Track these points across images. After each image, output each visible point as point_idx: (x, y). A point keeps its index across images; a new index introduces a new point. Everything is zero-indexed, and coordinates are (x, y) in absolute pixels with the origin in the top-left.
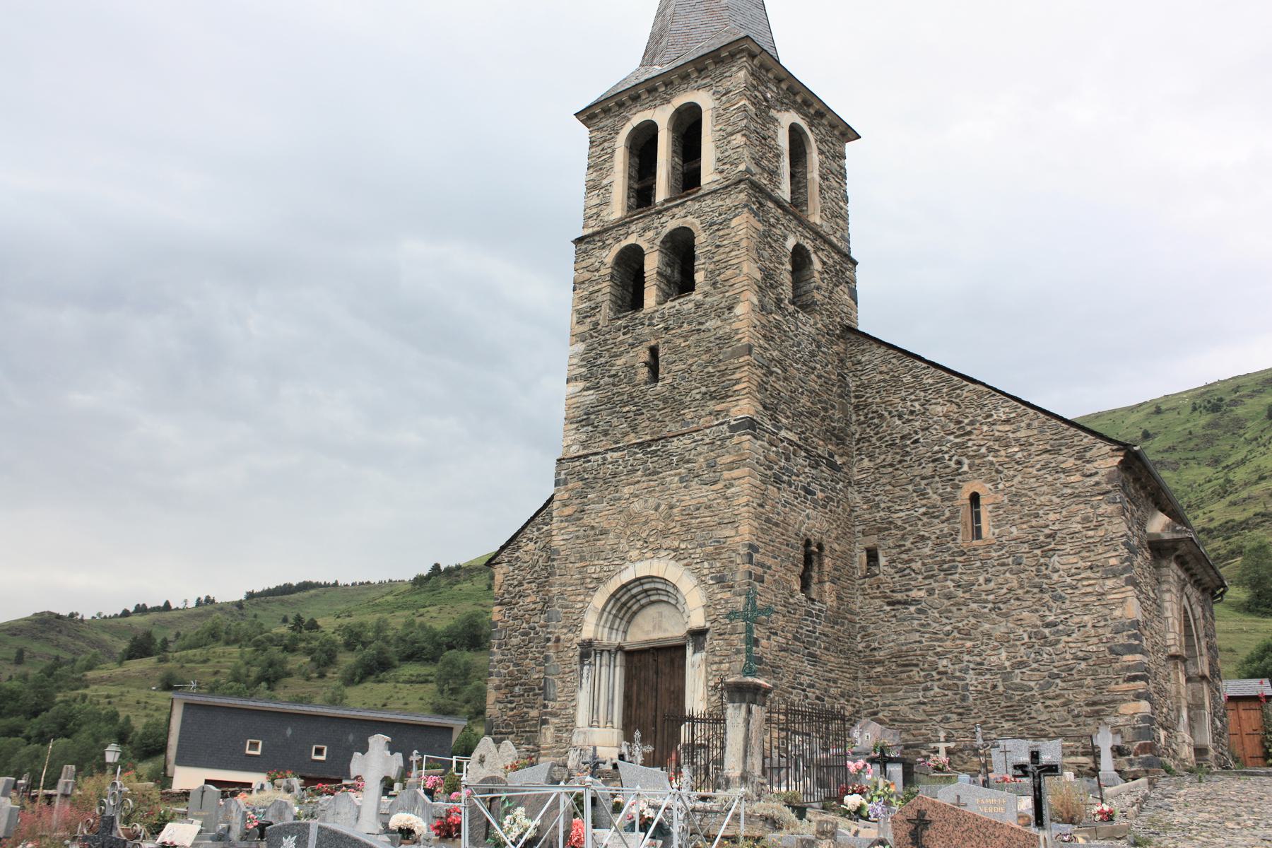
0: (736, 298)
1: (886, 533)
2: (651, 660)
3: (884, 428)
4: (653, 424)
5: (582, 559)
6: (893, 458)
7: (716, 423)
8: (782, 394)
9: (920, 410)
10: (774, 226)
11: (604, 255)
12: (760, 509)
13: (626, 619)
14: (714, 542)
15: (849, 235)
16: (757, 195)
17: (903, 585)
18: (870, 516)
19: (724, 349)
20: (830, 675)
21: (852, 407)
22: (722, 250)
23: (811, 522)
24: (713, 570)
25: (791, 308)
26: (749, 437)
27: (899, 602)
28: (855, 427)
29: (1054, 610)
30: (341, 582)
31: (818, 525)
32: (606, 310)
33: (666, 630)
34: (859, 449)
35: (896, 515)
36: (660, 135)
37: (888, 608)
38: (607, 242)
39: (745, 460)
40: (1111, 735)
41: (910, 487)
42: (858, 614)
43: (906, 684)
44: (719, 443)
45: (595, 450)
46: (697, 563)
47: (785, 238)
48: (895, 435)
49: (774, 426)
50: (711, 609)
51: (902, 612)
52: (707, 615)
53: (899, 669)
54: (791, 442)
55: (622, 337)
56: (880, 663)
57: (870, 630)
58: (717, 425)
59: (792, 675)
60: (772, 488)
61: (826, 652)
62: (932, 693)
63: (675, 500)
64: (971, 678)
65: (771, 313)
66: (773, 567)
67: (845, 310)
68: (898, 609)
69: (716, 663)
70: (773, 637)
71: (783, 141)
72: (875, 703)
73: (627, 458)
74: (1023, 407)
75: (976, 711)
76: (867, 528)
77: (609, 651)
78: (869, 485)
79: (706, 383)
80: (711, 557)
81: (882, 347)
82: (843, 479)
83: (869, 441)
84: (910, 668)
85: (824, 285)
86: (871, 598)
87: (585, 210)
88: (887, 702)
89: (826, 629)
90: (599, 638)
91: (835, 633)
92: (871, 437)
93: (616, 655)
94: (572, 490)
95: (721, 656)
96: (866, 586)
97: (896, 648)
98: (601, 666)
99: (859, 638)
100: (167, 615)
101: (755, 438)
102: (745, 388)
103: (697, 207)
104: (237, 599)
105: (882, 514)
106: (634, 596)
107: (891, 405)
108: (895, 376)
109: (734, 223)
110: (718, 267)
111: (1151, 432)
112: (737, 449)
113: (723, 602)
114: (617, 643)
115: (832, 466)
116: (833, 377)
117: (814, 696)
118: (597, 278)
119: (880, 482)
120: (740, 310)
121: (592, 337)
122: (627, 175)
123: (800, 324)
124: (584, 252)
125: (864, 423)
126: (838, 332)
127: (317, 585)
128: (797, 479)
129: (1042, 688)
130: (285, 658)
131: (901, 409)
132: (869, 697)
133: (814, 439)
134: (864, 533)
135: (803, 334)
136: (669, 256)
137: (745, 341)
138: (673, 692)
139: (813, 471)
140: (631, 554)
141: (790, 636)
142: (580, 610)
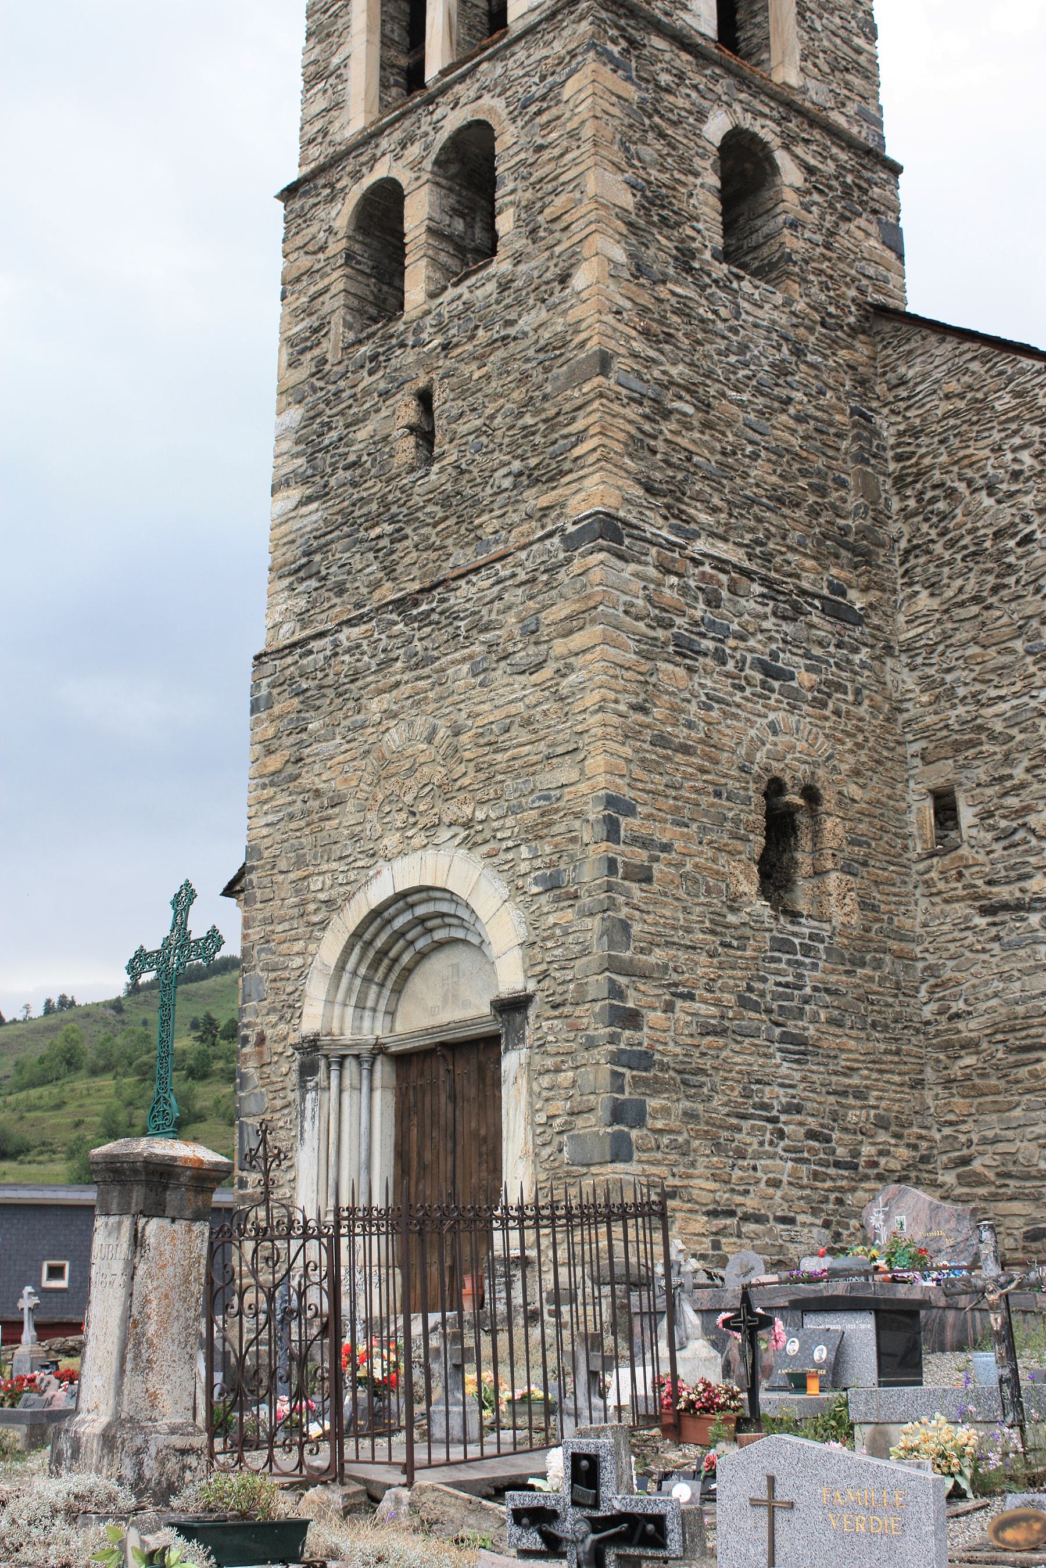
0: (575, 253)
1: (971, 753)
2: (442, 1072)
3: (959, 518)
4: (425, 555)
5: (300, 862)
7: (540, 533)
8: (695, 459)
9: (1032, 467)
10: (668, 90)
11: (333, 214)
12: (640, 717)
13: (390, 984)
14: (540, 798)
15: (880, 109)
16: (622, 22)
17: (1013, 868)
18: (935, 718)
19: (555, 371)
20: (847, 1081)
21: (890, 482)
22: (546, 155)
23: (782, 738)
24: (538, 863)
25: (721, 270)
26: (602, 556)
27: (1005, 907)
28: (899, 524)
31: (801, 745)
32: (338, 331)
33: (466, 1004)
34: (906, 572)
35: (988, 712)
37: (981, 921)
38: (339, 186)
39: (595, 608)
41: (1019, 645)
42: (917, 940)
43: (1029, 1091)
44: (545, 577)
45: (321, 628)
46: (508, 849)
47: (702, 116)
48: (982, 532)
49: (676, 530)
50: (537, 950)
51: (1012, 927)
53: (1012, 1059)
54: (721, 564)
55: (368, 380)
56: (970, 1045)
57: (947, 974)
58: (541, 539)
59: (739, 1088)
60: (670, 667)
61: (833, 1029)
63: (464, 715)
65: (664, 282)
66: (678, 845)
67: (871, 271)
68: (1003, 923)
69: (548, 1071)
70: (679, 1004)
72: (963, 1138)
73: (376, 636)
76: (931, 746)
77: (357, 1057)
78: (931, 648)
79: (519, 451)
80: (534, 834)
81: (949, 339)
82: (870, 641)
83: (928, 552)
86: (946, 901)
87: (302, 129)
88: (990, 1134)
89: (833, 978)
90: (336, 1030)
92: (932, 541)
93: (372, 1065)
94: (280, 717)
96: (934, 874)
97: (1003, 1010)
98: (341, 1091)
99: (923, 994)
101: (621, 557)
102: (594, 450)
103: (499, 71)
104: (113, 997)
105: (961, 710)
106: (400, 934)
107: (971, 465)
108: (977, 401)
109: (567, 92)
110: (539, 195)
112: (578, 585)
114: (370, 1038)
116: (838, 417)
117: (802, 1131)
118: (322, 264)
119: (953, 640)
120: (580, 280)
121: (314, 390)
122: (377, 38)
123: (745, 305)
124: (299, 216)
126: (852, 319)
128: (742, 645)
130: (191, 1089)
131: (991, 472)
132: (951, 1123)
133: (790, 556)
134: (924, 757)
135: (756, 326)
136: (459, 195)
137: (592, 346)
138: (485, 1140)
139: (787, 627)
140: (385, 841)
141: (729, 998)
142: (298, 973)
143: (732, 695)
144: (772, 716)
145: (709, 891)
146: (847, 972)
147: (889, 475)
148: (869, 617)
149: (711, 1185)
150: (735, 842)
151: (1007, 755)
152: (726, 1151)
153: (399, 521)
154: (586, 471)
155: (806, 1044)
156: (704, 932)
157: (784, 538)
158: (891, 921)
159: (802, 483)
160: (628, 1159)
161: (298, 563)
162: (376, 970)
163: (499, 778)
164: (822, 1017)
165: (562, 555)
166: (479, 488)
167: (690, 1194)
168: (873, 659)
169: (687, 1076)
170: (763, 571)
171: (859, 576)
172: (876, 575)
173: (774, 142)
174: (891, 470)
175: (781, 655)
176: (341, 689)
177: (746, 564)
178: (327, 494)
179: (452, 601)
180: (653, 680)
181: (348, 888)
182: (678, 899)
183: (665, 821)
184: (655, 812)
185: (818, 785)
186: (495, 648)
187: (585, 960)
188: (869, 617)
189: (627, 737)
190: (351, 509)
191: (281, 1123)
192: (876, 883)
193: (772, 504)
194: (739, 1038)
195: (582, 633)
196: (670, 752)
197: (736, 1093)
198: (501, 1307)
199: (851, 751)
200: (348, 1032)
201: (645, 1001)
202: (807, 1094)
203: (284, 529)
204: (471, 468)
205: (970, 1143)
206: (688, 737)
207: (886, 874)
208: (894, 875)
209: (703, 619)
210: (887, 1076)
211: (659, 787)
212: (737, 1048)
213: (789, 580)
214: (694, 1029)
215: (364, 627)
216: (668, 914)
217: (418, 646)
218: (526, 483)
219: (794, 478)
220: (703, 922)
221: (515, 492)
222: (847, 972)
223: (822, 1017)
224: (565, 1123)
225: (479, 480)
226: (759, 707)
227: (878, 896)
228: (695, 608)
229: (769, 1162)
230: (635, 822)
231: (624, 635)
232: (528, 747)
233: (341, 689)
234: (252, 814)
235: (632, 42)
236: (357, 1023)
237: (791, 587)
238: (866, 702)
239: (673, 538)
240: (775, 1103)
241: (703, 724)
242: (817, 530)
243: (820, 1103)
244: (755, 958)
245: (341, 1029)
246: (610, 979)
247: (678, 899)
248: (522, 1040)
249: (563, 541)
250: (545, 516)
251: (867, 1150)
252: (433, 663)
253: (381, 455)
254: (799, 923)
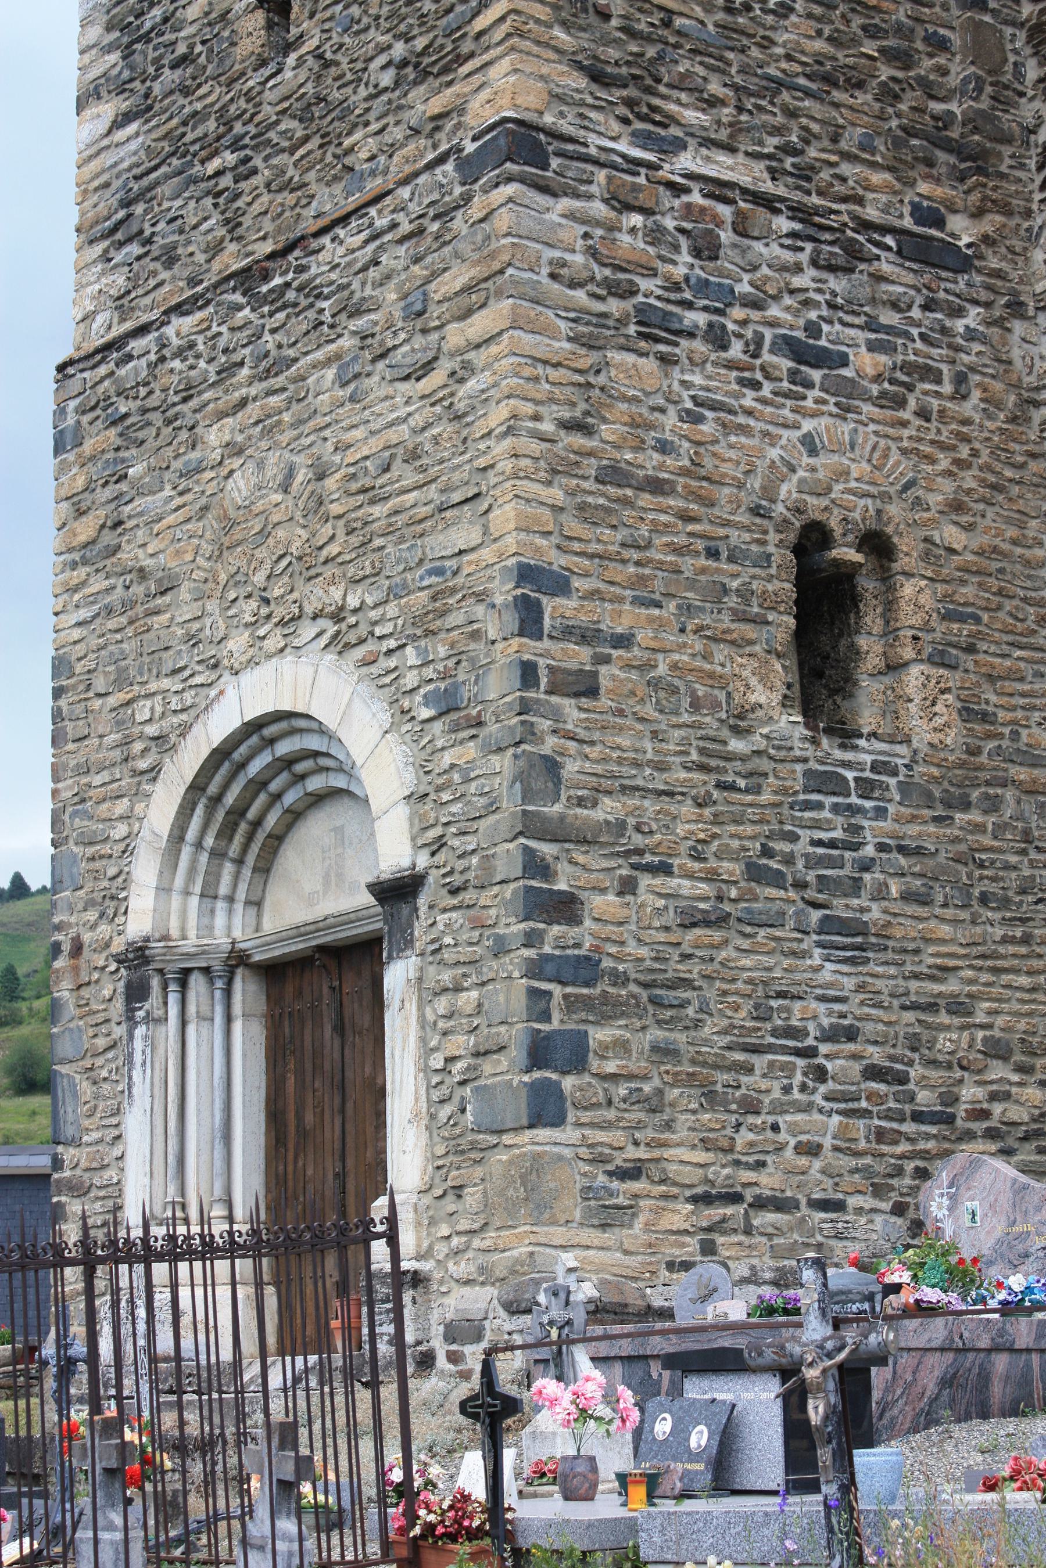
2: (326, 990)
5: (121, 681)
7: (430, 156)
8: (678, 22)
12: (578, 440)
13: (251, 859)
20: (937, 988)
21: (1022, 35)
24: (429, 672)
39: (501, 272)
44: (435, 227)
45: (145, 318)
46: (390, 652)
49: (643, 140)
50: (430, 805)
58: (430, 166)
59: (747, 1006)
60: (631, 358)
63: (329, 446)
66: (643, 636)
69: (446, 990)
70: (645, 881)
73: (215, 329)
77: (206, 970)
79: (402, 27)
82: (984, 296)
89: (913, 829)
90: (174, 933)
91: (956, 840)
93: (230, 982)
94: (92, 458)
95: (458, 963)
98: (184, 1023)
100: (20, 907)
101: (544, 189)
102: (502, 19)
106: (259, 784)
112: (479, 238)
113: (456, 777)
117: (857, 1067)
128: (755, 315)
133: (846, 169)
139: (837, 284)
140: (231, 645)
141: (729, 868)
142: (121, 846)
143: (738, 396)
145: (696, 705)
146: (936, 819)
147: (1022, 25)
148: (981, 257)
149: (701, 1156)
150: (742, 626)
152: (725, 1103)
153: (245, 147)
154: (493, 53)
155: (865, 934)
156: (688, 769)
157: (835, 139)
158: (1015, 736)
159: (869, 48)
160: (558, 1121)
161: (114, 219)
162: (231, 839)
163: (378, 542)
164: (894, 890)
165: (458, 190)
166: (349, 90)
167: (664, 1170)
168: (988, 324)
169: (658, 992)
170: (797, 196)
171: (967, 192)
172: (995, 189)
174: (1025, 15)
175: (825, 328)
176: (170, 413)
177: (768, 186)
178: (150, 108)
179: (313, 270)
180: (601, 380)
181: (184, 717)
182: (642, 720)
183: (621, 600)
184: (602, 586)
185: (889, 530)
186: (369, 341)
187: (492, 819)
188: (981, 257)
189: (555, 472)
190: (182, 130)
191: (104, 1073)
192: (991, 678)
193: (814, 86)
194: (748, 929)
195: (484, 312)
196: (629, 492)
197: (743, 1014)
198: (384, 1348)
199: (948, 473)
200: (192, 933)
201: (584, 879)
202: (867, 1010)
203: (94, 165)
204: (339, 57)
206: (661, 467)
207: (1008, 663)
208: (1022, 665)
209: (687, 279)
210: (1006, 978)
211: (610, 548)
212: (745, 944)
213: (842, 207)
214: (670, 918)
215: (199, 315)
216: (624, 742)
217: (269, 341)
218: (412, 77)
219: (855, 42)
220: (687, 753)
221: (397, 93)
222: (936, 819)
223: (894, 890)
224: (468, 1069)
225: (349, 76)
226: (786, 412)
227: (993, 698)
228: (674, 263)
229: (799, 1117)
230: (568, 605)
231: (550, 313)
232: (415, 494)
233: (170, 413)
234: (59, 609)
236: (206, 921)
237: (845, 218)
238: (976, 394)
239: (637, 153)
240: (811, 1027)
241: (686, 445)
242: (894, 123)
243: (889, 1024)
244: (775, 805)
245: (183, 929)
246: (526, 848)
247: (642, 720)
248: (409, 943)
249: (458, 168)
250: (437, 129)
251: (970, 1093)
252: (288, 367)
253: (219, 43)
254: (855, 748)
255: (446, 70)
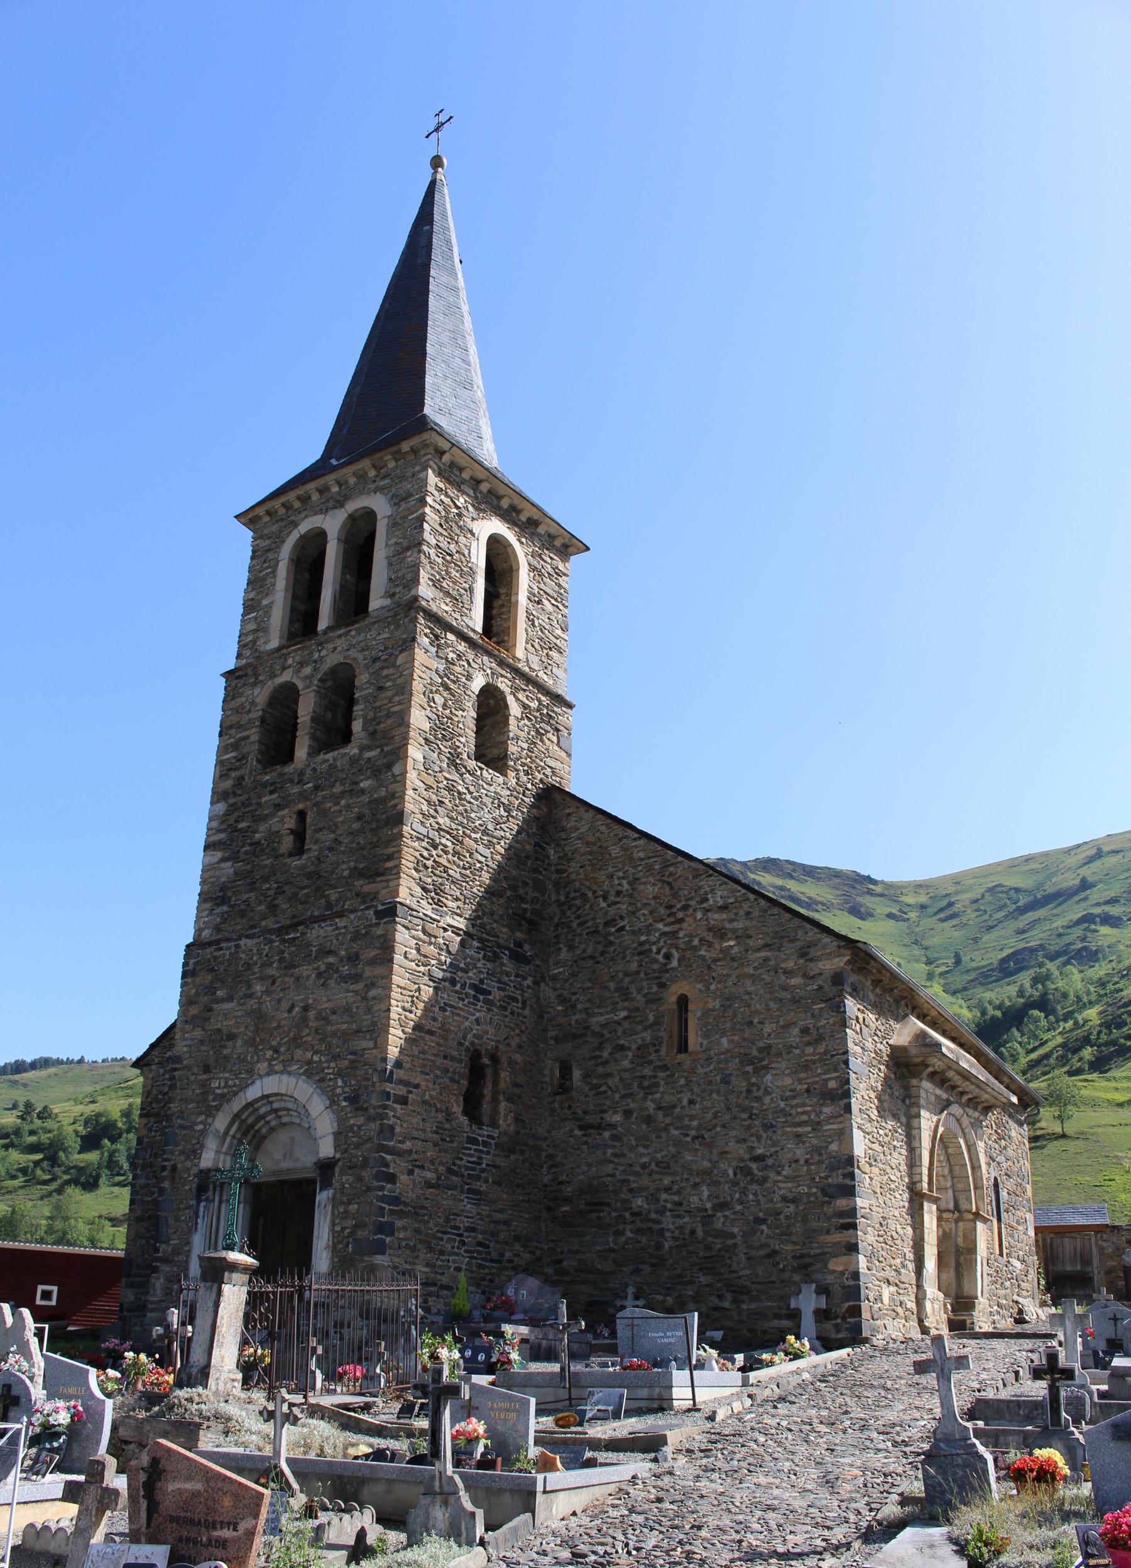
1: (581, 1041)
6: (595, 949)
11: (256, 693)
24: (347, 1089)
25: (472, 764)
27: (592, 1127)
29: (763, 1141)
30: (89, 1058)
32: (252, 761)
36: (328, 546)
37: (577, 1132)
40: (814, 1296)
47: (469, 677)
52: (337, 1147)
56: (568, 1200)
57: (558, 1159)
62: (623, 1239)
64: (668, 1222)
70: (417, 1171)
71: (479, 557)
72: (559, 1250)
74: (743, 891)
75: (671, 1261)
78: (566, 981)
83: (569, 927)
84: (600, 1207)
85: (523, 734)
98: (220, 1202)
111: (1090, 879)
115: (518, 957)
121: (235, 795)
125: (564, 903)
127: (59, 1062)
129: (745, 1235)
132: (553, 1241)
134: (557, 1039)
141: (442, 1169)
144: (478, 1015)
145: (437, 1111)
151: (601, 1043)
173: (507, 690)
205: (562, 1252)
235: (437, 637)
239: (434, 916)
251: (508, 1254)
255: (371, 877)
